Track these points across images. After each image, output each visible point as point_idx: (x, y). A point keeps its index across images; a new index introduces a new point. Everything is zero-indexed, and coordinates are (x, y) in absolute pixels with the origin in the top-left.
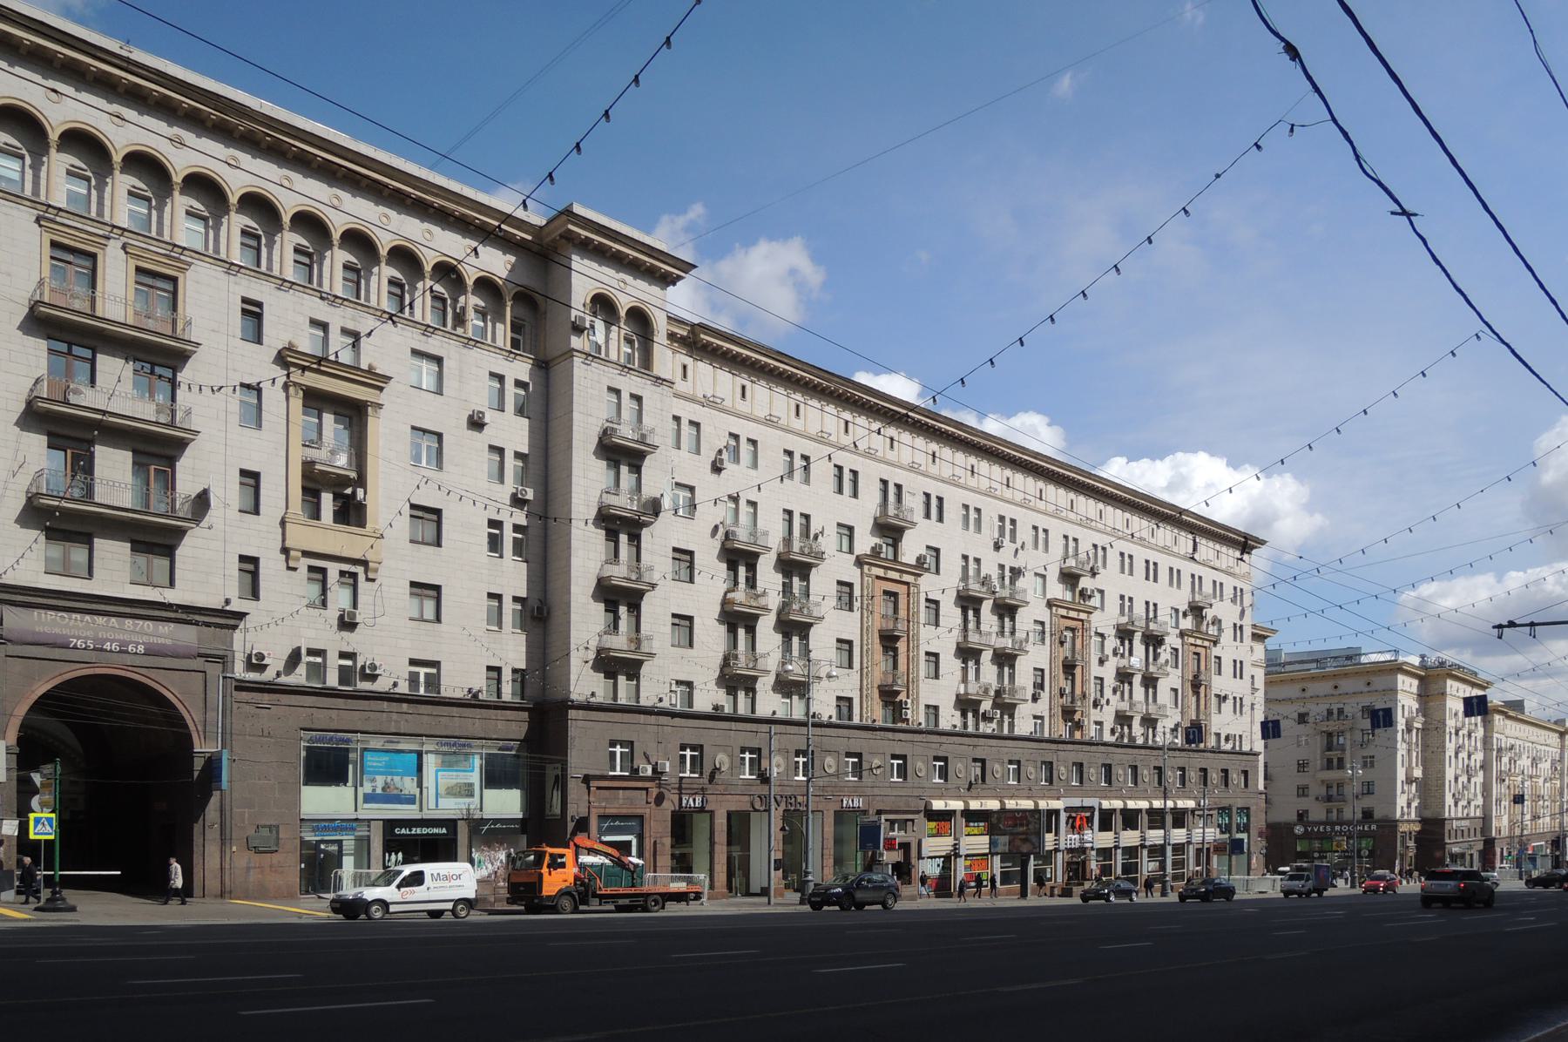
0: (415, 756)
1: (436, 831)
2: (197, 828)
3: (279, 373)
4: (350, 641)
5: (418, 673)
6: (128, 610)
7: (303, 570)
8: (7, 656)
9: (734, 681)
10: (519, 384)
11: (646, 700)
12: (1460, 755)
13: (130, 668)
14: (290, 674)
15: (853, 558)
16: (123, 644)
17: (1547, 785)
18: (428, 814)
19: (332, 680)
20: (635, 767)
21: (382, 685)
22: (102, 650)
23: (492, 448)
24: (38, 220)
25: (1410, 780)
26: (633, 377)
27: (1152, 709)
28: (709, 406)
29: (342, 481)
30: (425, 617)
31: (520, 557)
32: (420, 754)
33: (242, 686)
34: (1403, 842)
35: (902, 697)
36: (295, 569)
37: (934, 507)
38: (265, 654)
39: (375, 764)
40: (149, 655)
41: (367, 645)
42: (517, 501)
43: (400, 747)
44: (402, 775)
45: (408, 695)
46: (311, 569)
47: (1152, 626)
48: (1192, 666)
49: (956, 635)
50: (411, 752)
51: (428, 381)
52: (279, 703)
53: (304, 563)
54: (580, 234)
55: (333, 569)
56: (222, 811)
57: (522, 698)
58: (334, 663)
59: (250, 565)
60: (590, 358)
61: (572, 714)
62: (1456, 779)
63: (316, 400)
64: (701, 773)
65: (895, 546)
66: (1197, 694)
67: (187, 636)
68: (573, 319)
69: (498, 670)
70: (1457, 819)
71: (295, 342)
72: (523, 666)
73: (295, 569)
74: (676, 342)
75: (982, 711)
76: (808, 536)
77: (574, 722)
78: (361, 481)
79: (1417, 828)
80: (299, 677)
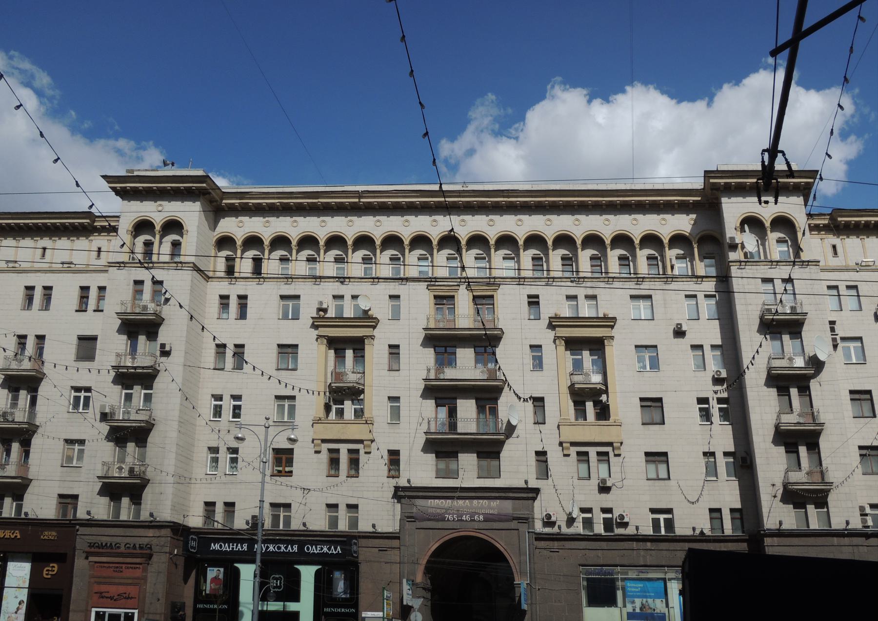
3: (551, 334)
4: (606, 500)
5: (659, 519)
6: (473, 494)
7: (574, 455)
8: (417, 529)
11: (837, 523)
13: (477, 531)
14: (571, 527)
19: (599, 529)
21: (630, 531)
23: (694, 347)
26: (782, 267)
28: (861, 270)
29: (600, 392)
30: (660, 477)
31: (727, 421)
32: (664, 580)
33: (540, 537)
36: (568, 455)
38: (551, 514)
39: (633, 590)
40: (487, 521)
41: (618, 502)
43: (650, 576)
44: (654, 598)
45: (271, 530)
50: (658, 579)
51: (644, 313)
52: (563, 548)
53: (573, 450)
54: (720, 183)
55: (592, 451)
57: (743, 532)
58: (599, 518)
59: (541, 455)
60: (743, 264)
63: (573, 345)
67: (507, 507)
69: (719, 510)
71: (558, 313)
72: (738, 505)
73: (568, 455)
74: (822, 231)
77: (770, 548)
80: (578, 528)
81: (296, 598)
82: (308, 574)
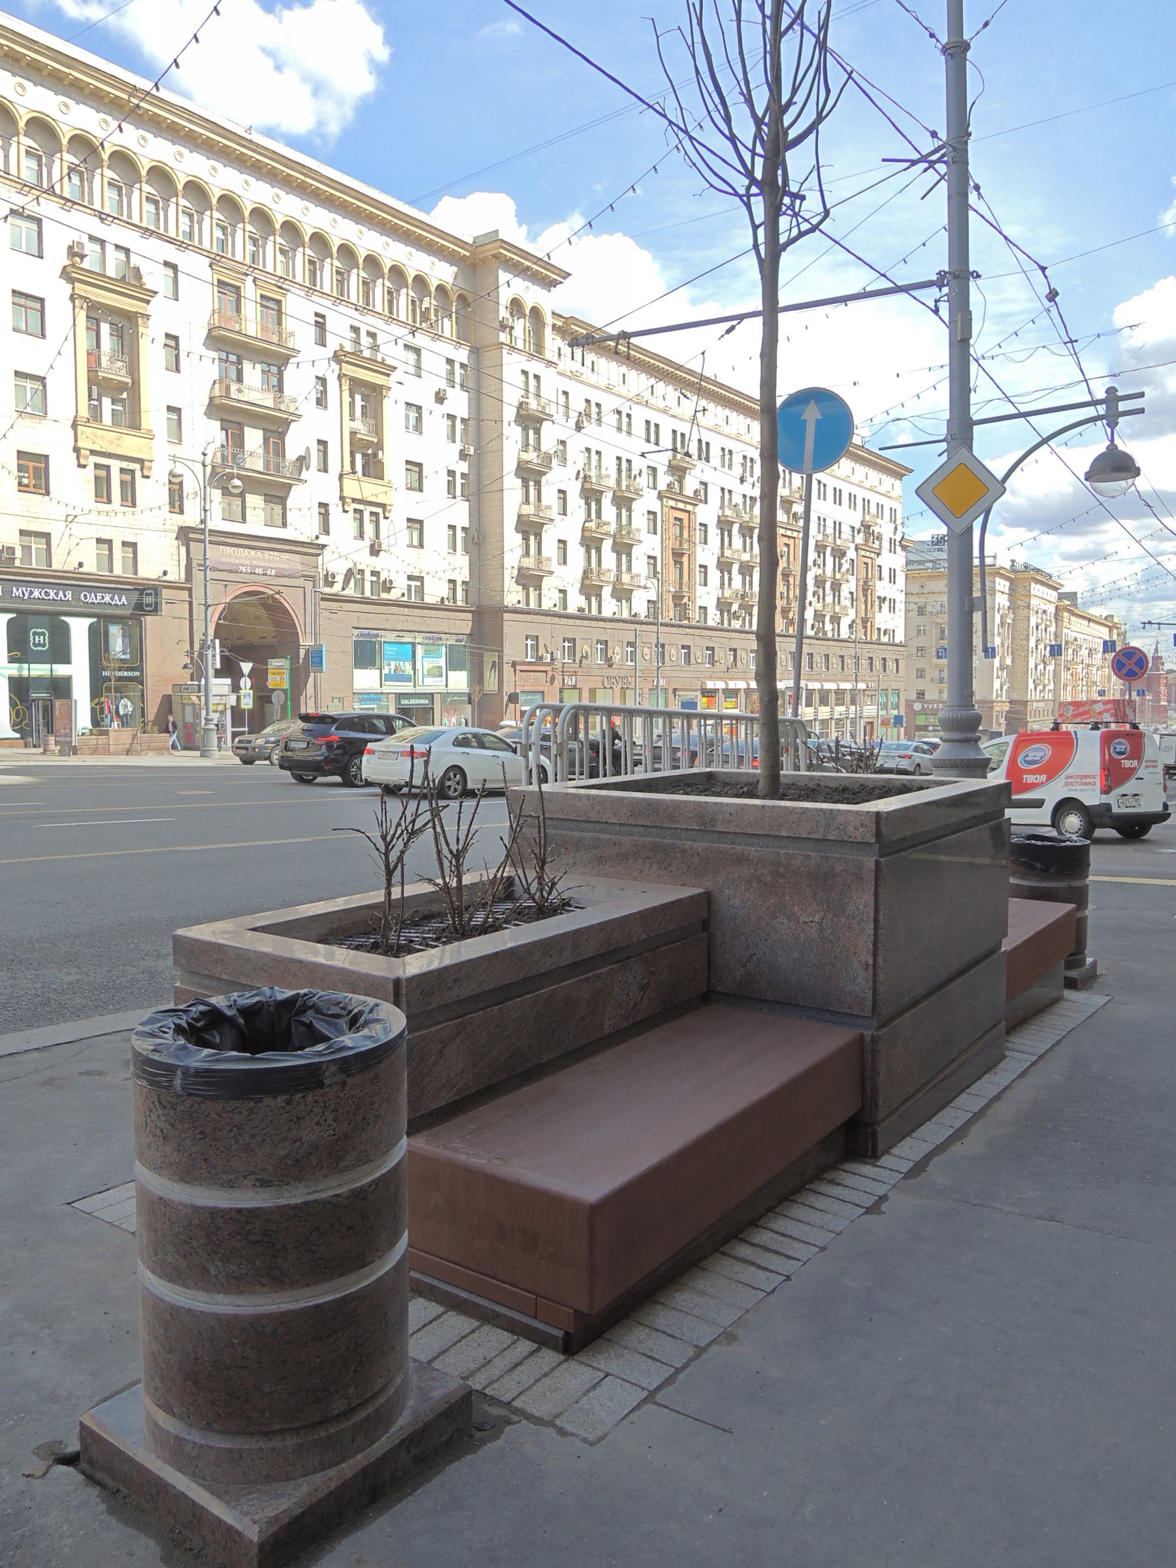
0: (410, 646)
1: (422, 701)
2: (302, 699)
4: (377, 563)
9: (590, 590)
10: (462, 365)
12: (1039, 647)
15: (656, 492)
16: (265, 568)
17: (1099, 672)
18: (419, 690)
20: (540, 655)
22: (254, 573)
24: (211, 265)
25: (1002, 667)
27: (837, 609)
32: (413, 644)
34: (997, 719)
35: (685, 600)
37: (704, 452)
42: (463, 456)
46: (356, 511)
47: (838, 542)
48: (863, 574)
49: (717, 551)
53: (351, 507)
56: (315, 686)
61: (506, 616)
62: (1036, 667)
64: (574, 660)
65: (681, 481)
66: (865, 596)
68: (501, 319)
70: (1036, 701)
73: (347, 512)
75: (733, 611)
76: (630, 477)
78: (379, 446)
79: (1007, 707)
81: (66, 660)
82: (79, 629)
